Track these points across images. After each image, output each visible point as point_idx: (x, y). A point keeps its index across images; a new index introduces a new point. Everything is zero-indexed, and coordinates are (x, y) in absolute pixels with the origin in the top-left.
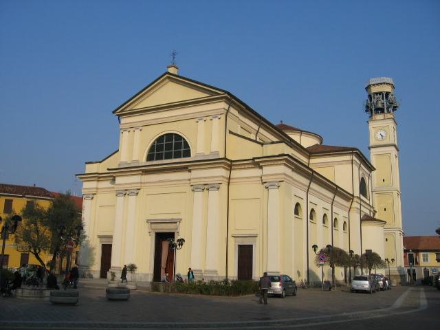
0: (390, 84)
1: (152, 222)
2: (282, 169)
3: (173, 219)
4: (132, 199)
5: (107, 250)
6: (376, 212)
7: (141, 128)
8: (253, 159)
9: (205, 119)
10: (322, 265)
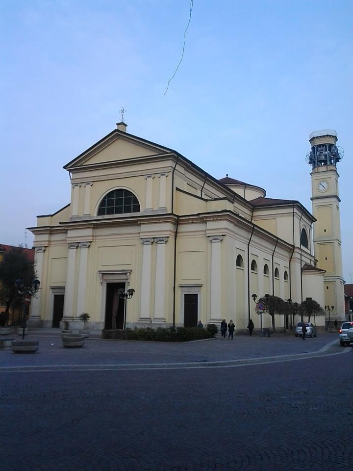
0: (333, 136)
1: (104, 274)
2: (224, 224)
3: (123, 270)
4: (84, 251)
5: (59, 301)
6: (317, 261)
7: (91, 183)
8: (199, 214)
9: (153, 176)
10: (261, 313)
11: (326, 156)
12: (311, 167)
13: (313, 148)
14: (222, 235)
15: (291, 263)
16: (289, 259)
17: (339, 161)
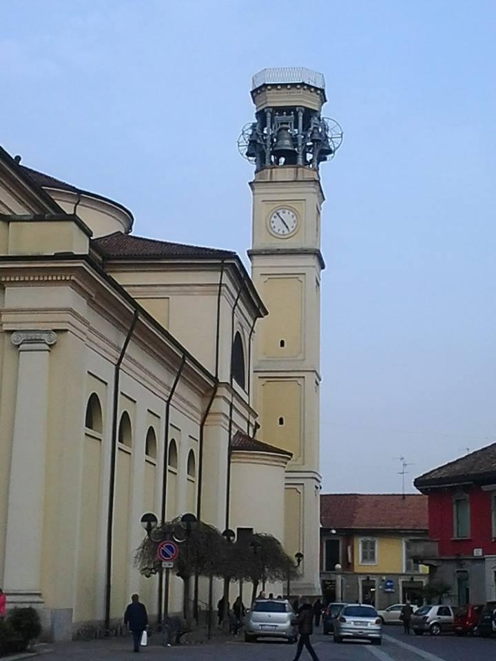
0: (316, 89)
11: (294, 139)
12: (251, 166)
13: (261, 115)
14: (55, 331)
15: (204, 428)
16: (200, 417)
17: (325, 159)
